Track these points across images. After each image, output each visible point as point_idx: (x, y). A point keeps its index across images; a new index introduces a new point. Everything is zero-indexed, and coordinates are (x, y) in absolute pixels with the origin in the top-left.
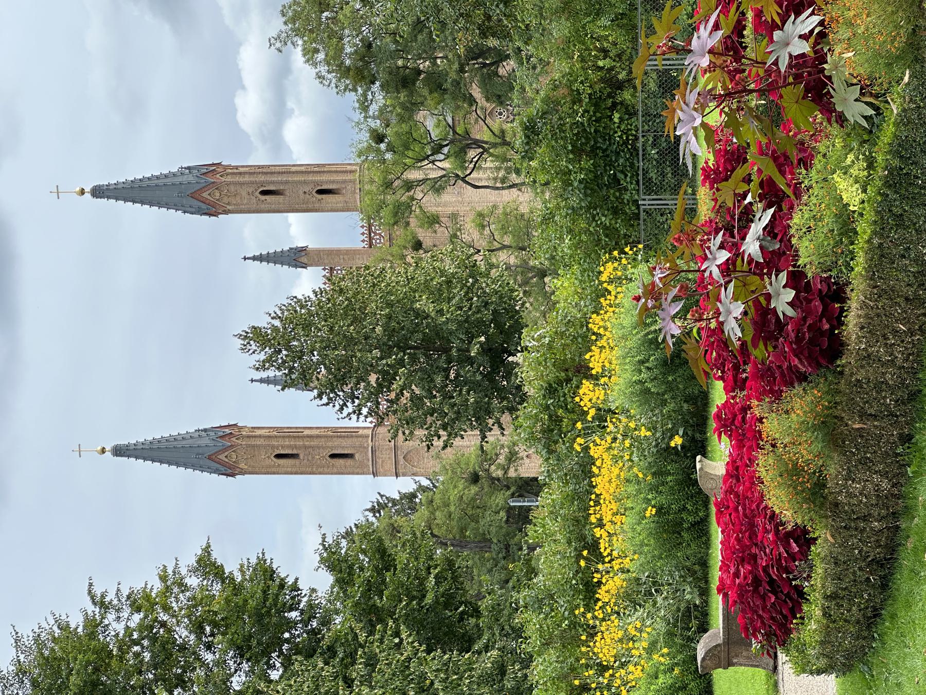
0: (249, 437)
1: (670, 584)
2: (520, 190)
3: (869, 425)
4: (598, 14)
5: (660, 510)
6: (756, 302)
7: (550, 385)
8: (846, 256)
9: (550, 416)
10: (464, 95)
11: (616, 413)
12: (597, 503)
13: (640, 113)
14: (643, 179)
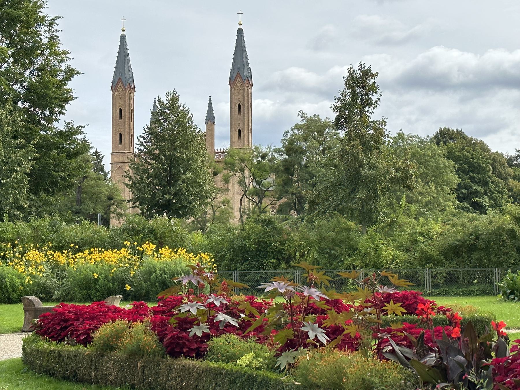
0: (129, 97)
1: (62, 285)
2: (239, 220)
3: (139, 370)
4: (319, 253)
5: (96, 280)
6: (196, 319)
7: (154, 231)
8: (216, 359)
9: (140, 231)
10: (282, 195)
11: (141, 260)
12: (100, 252)
13: (275, 271)
14: (246, 273)
